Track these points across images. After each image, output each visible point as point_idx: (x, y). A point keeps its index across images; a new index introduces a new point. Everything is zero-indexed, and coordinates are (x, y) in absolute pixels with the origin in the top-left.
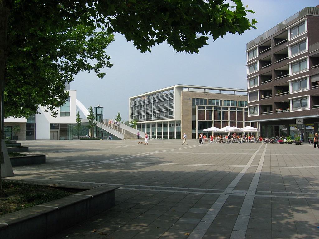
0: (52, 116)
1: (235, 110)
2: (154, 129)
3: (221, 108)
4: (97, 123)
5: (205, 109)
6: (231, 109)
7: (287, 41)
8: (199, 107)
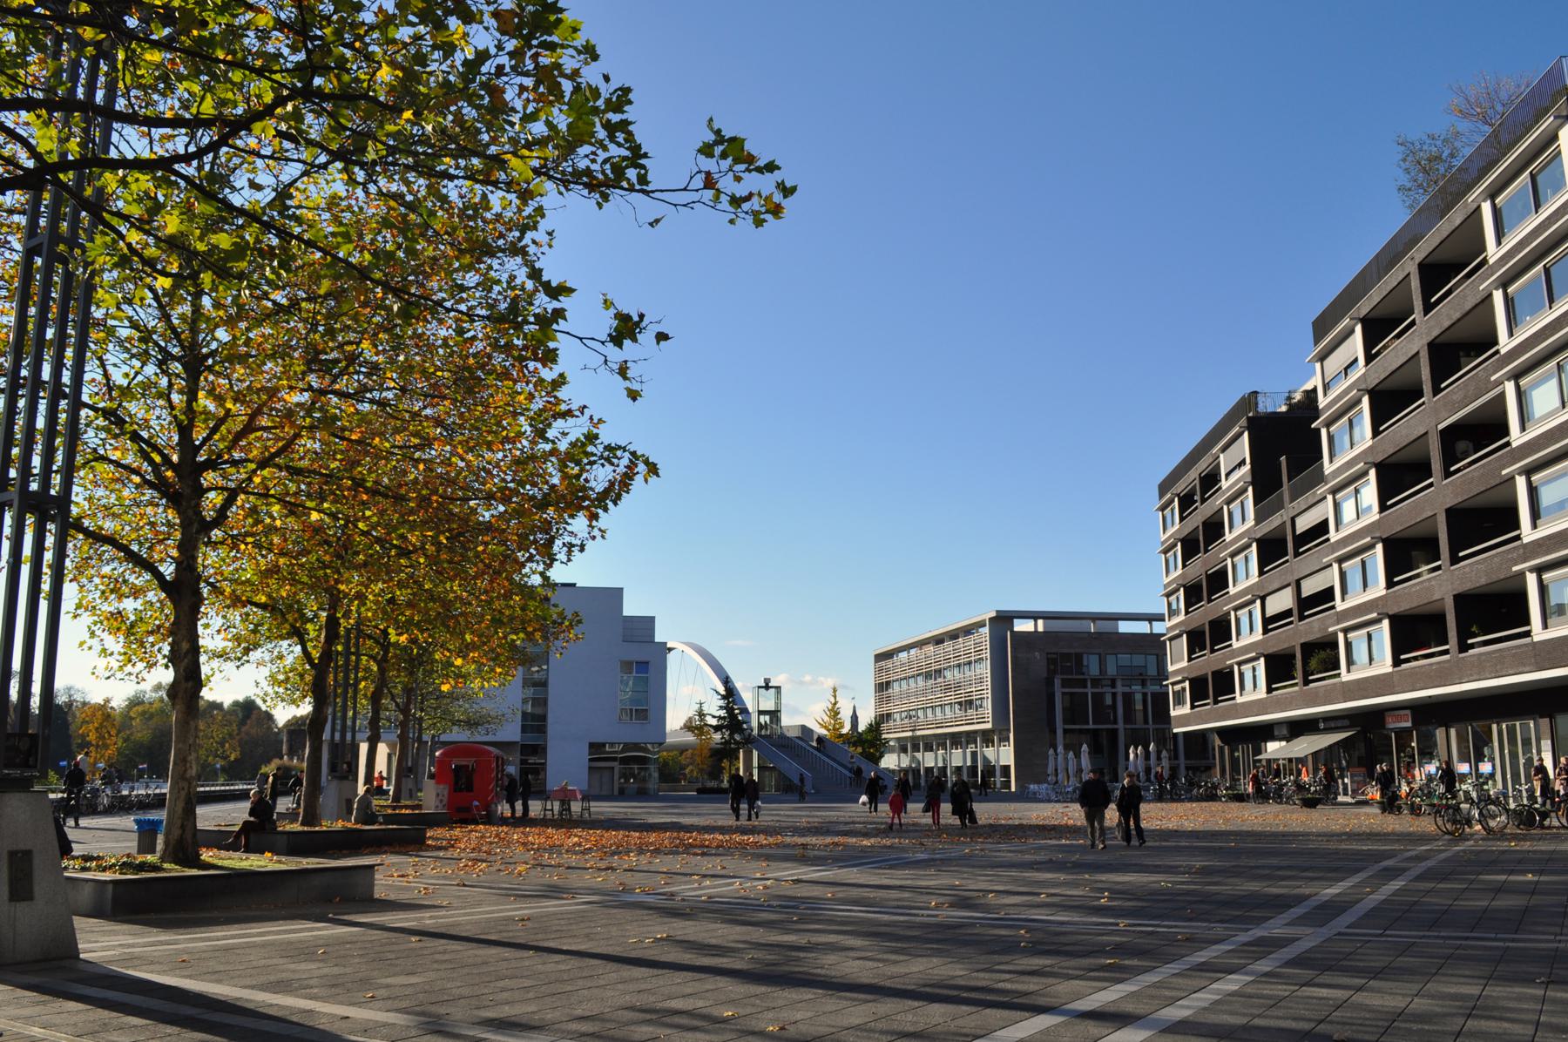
7: (1485, 261)
8: (1065, 683)
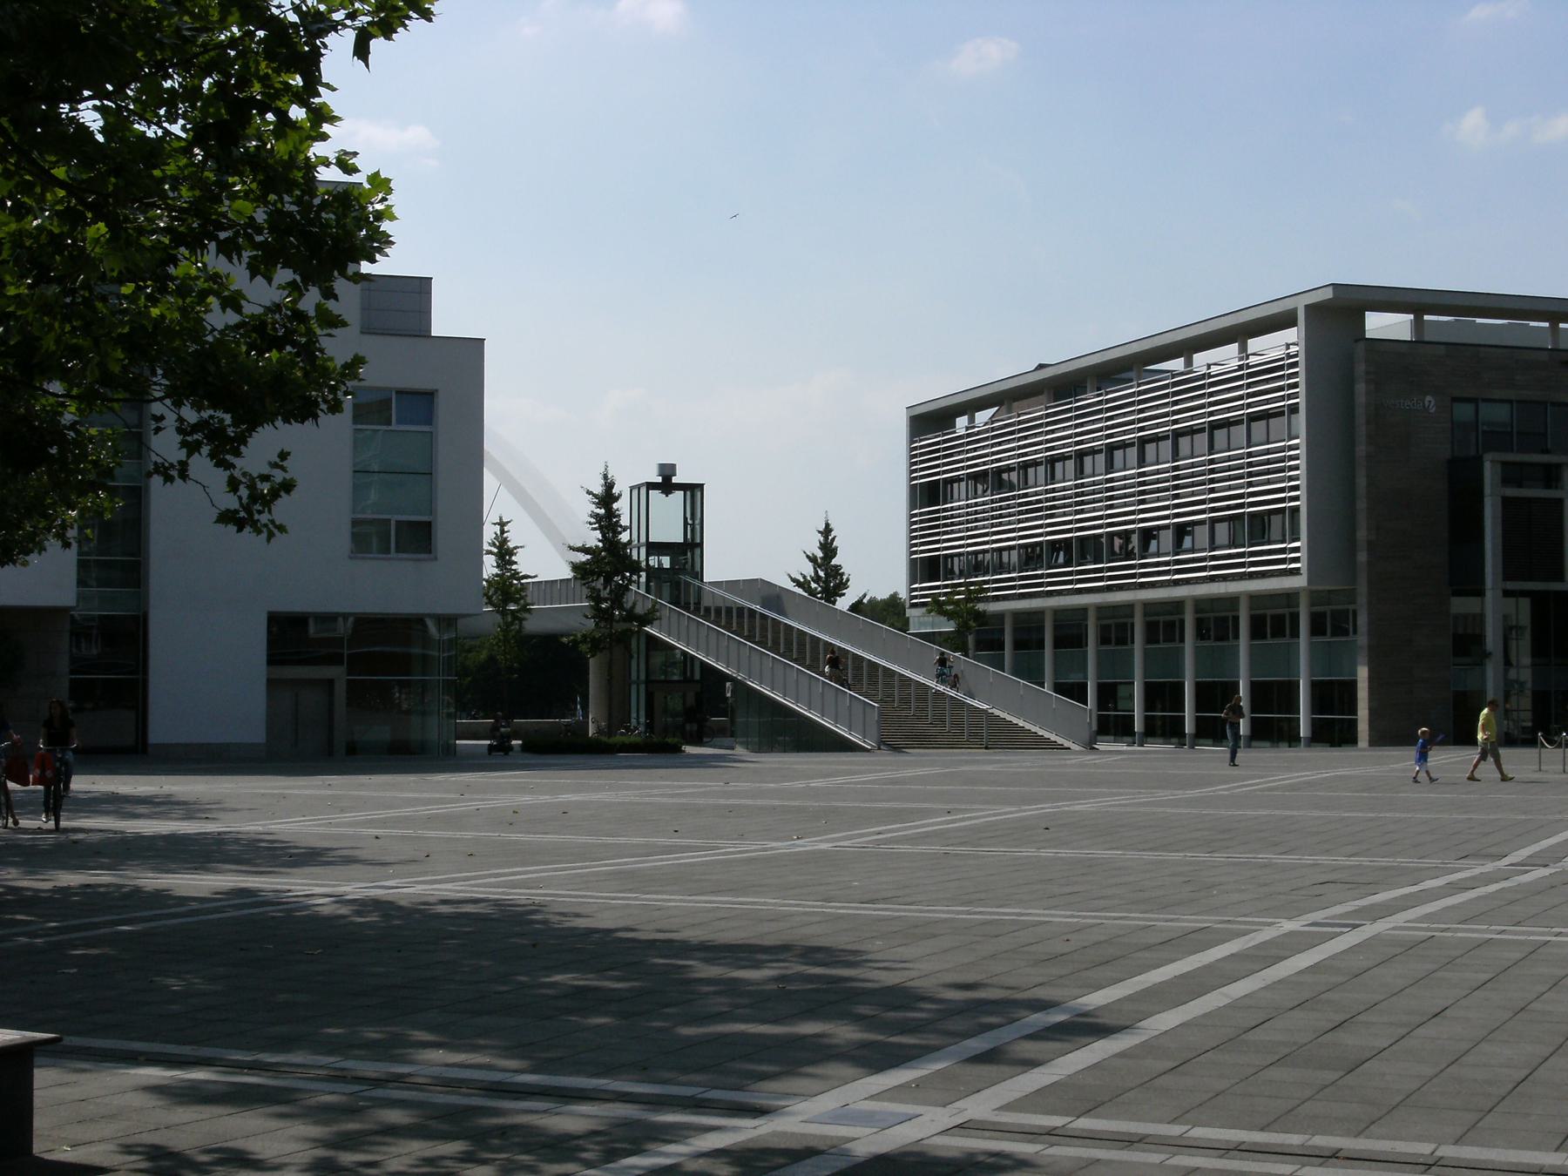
0: (226, 517)
2: (1115, 663)
4: (653, 610)
8: (1512, 475)
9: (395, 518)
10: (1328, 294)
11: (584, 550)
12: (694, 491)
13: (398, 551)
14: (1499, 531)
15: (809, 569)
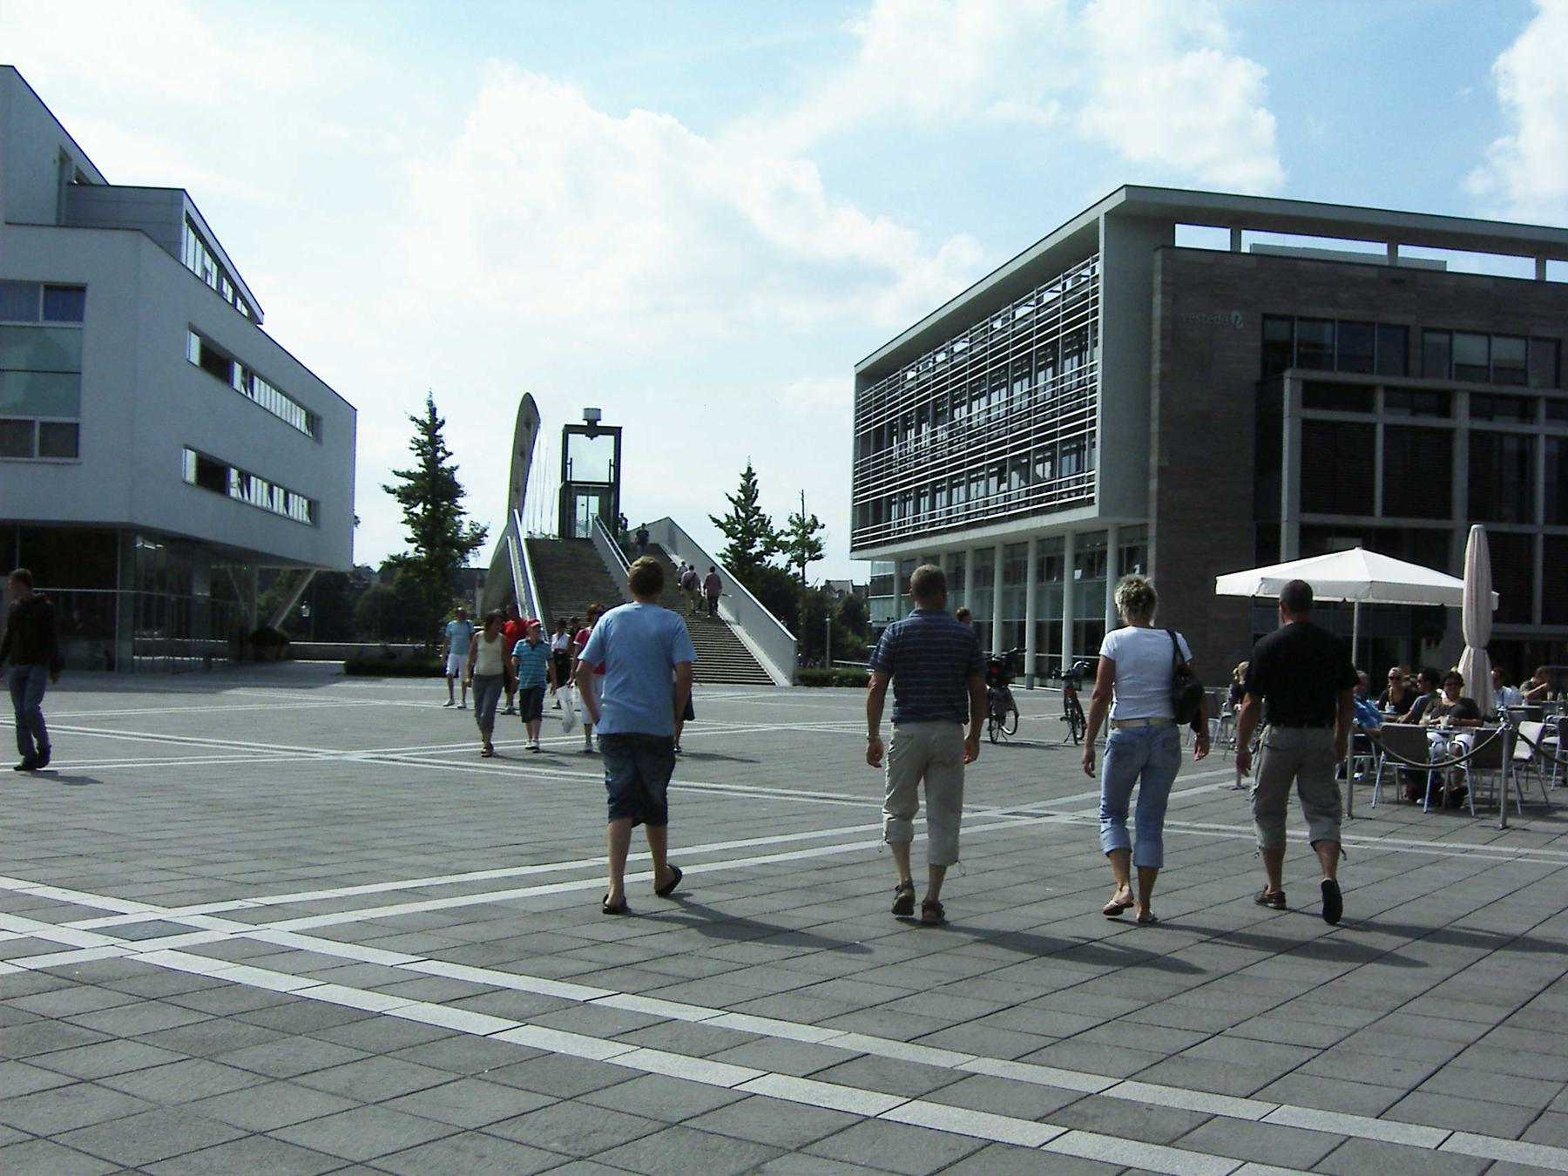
1: (1368, 407)
3: (1380, 398)
5: (1381, 417)
6: (1483, 405)
8: (1313, 394)
9: (38, 419)
10: (1121, 198)
11: (408, 475)
12: (616, 432)
13: (42, 453)
14: (1298, 457)
15: (730, 509)
